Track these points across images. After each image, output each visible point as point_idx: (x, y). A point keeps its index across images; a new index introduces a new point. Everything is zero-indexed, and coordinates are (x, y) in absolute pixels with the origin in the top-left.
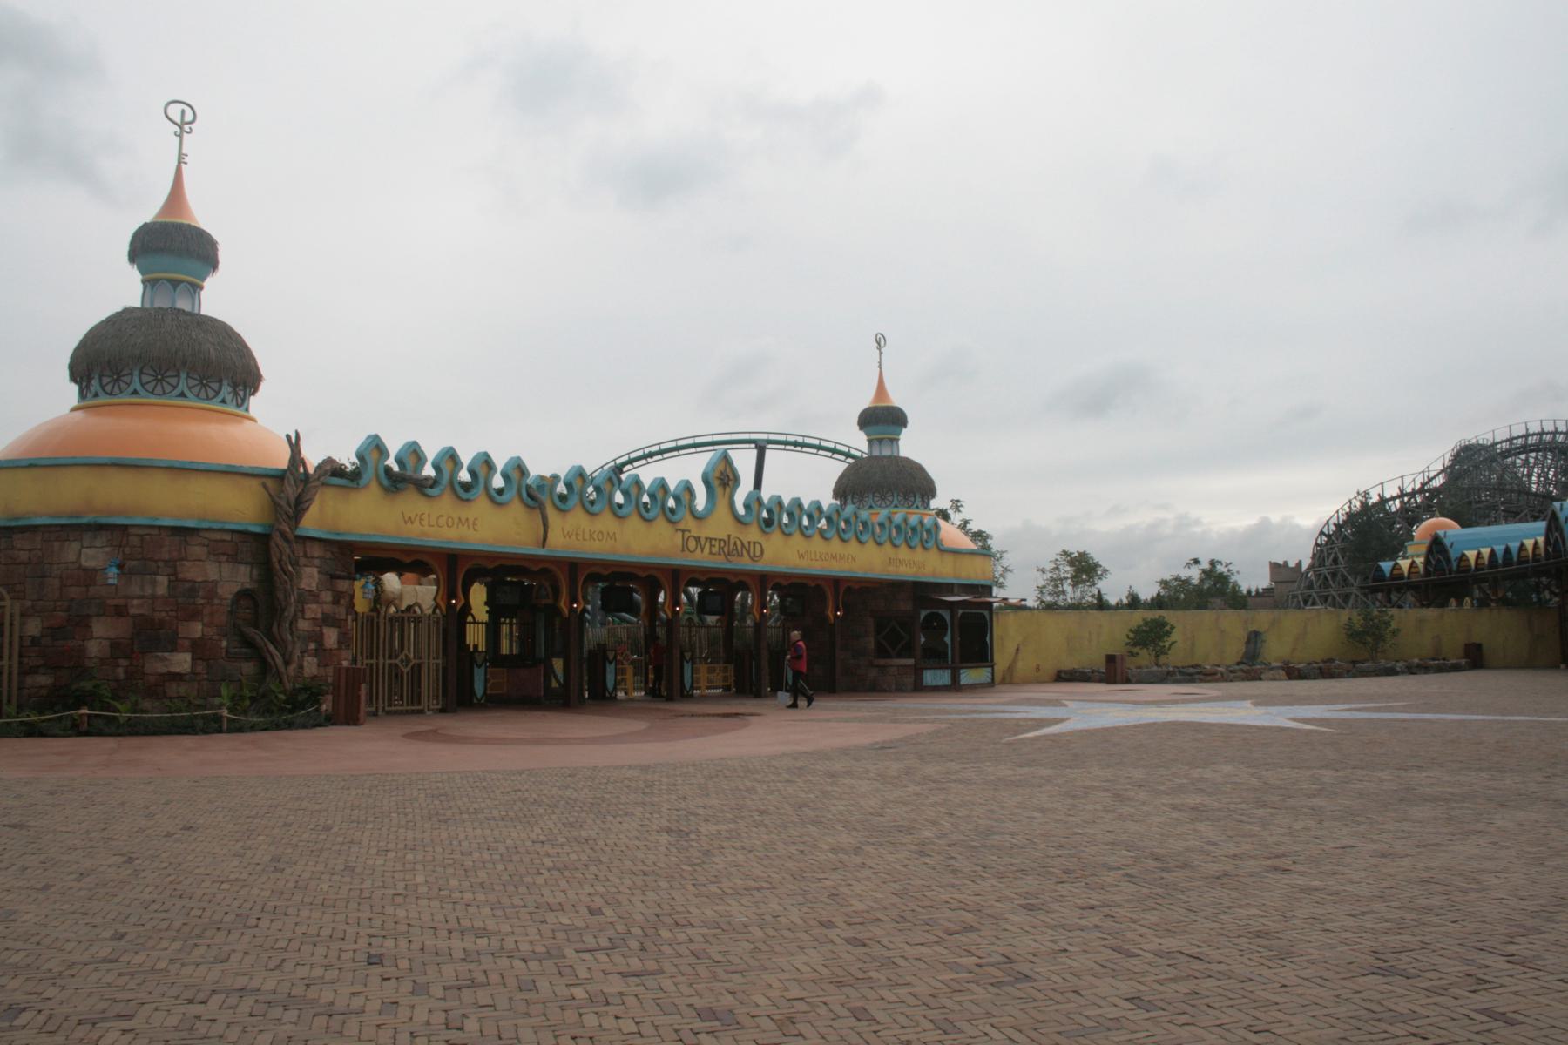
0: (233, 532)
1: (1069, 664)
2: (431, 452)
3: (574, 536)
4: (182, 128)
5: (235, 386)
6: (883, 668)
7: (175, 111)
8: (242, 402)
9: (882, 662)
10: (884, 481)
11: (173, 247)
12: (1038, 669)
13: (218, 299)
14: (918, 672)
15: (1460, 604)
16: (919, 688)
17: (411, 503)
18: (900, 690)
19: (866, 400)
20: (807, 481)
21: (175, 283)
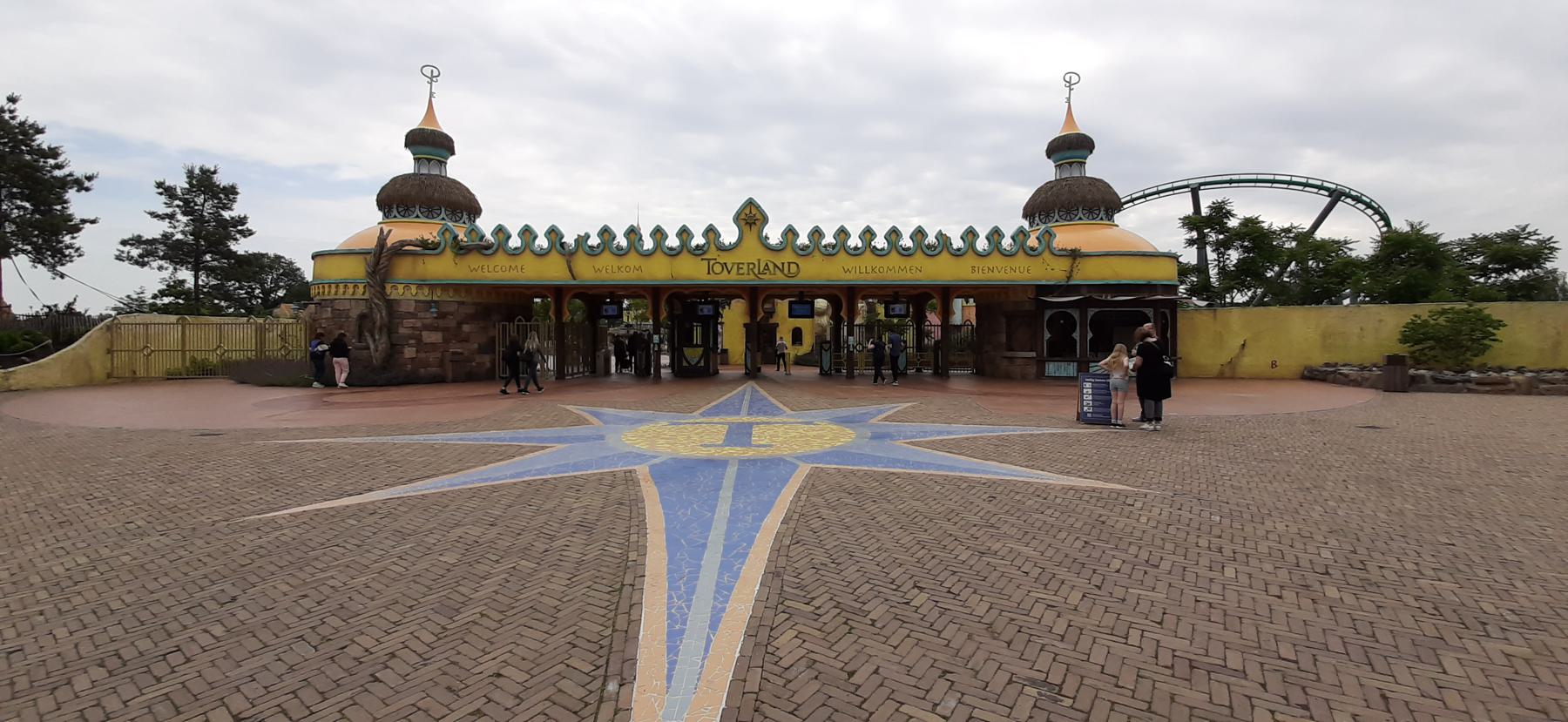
0: (445, 287)
1: (1318, 359)
2: (514, 229)
3: (590, 272)
4: (432, 79)
5: (1106, 211)
6: (1011, 359)
7: (427, 71)
8: (1110, 218)
9: (1009, 354)
10: (425, 188)
11: (430, 143)
12: (1274, 365)
13: (455, 169)
14: (1041, 363)
15: (790, 232)
16: (1041, 376)
17: (474, 261)
18: (1024, 379)
19: (415, 121)
20: (1001, 206)
21: (1071, 164)
